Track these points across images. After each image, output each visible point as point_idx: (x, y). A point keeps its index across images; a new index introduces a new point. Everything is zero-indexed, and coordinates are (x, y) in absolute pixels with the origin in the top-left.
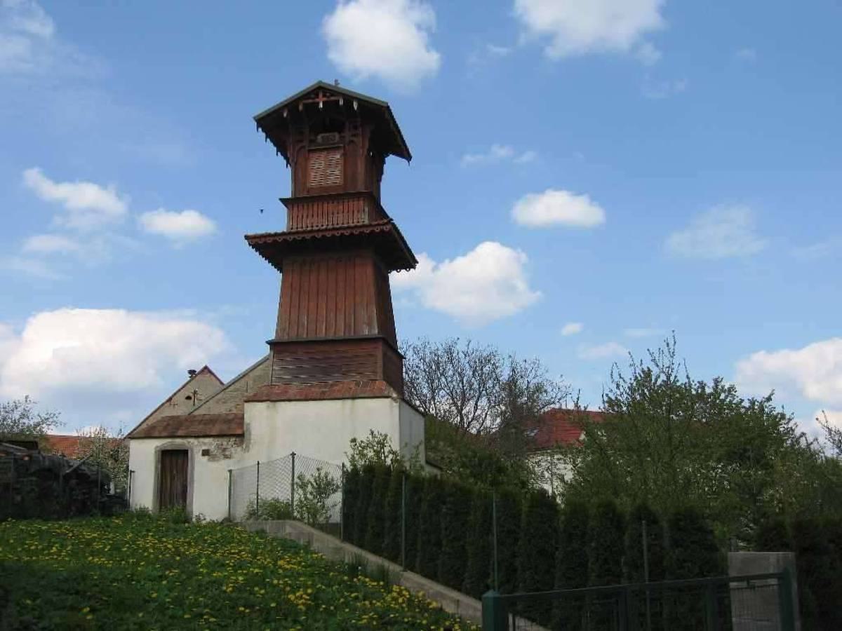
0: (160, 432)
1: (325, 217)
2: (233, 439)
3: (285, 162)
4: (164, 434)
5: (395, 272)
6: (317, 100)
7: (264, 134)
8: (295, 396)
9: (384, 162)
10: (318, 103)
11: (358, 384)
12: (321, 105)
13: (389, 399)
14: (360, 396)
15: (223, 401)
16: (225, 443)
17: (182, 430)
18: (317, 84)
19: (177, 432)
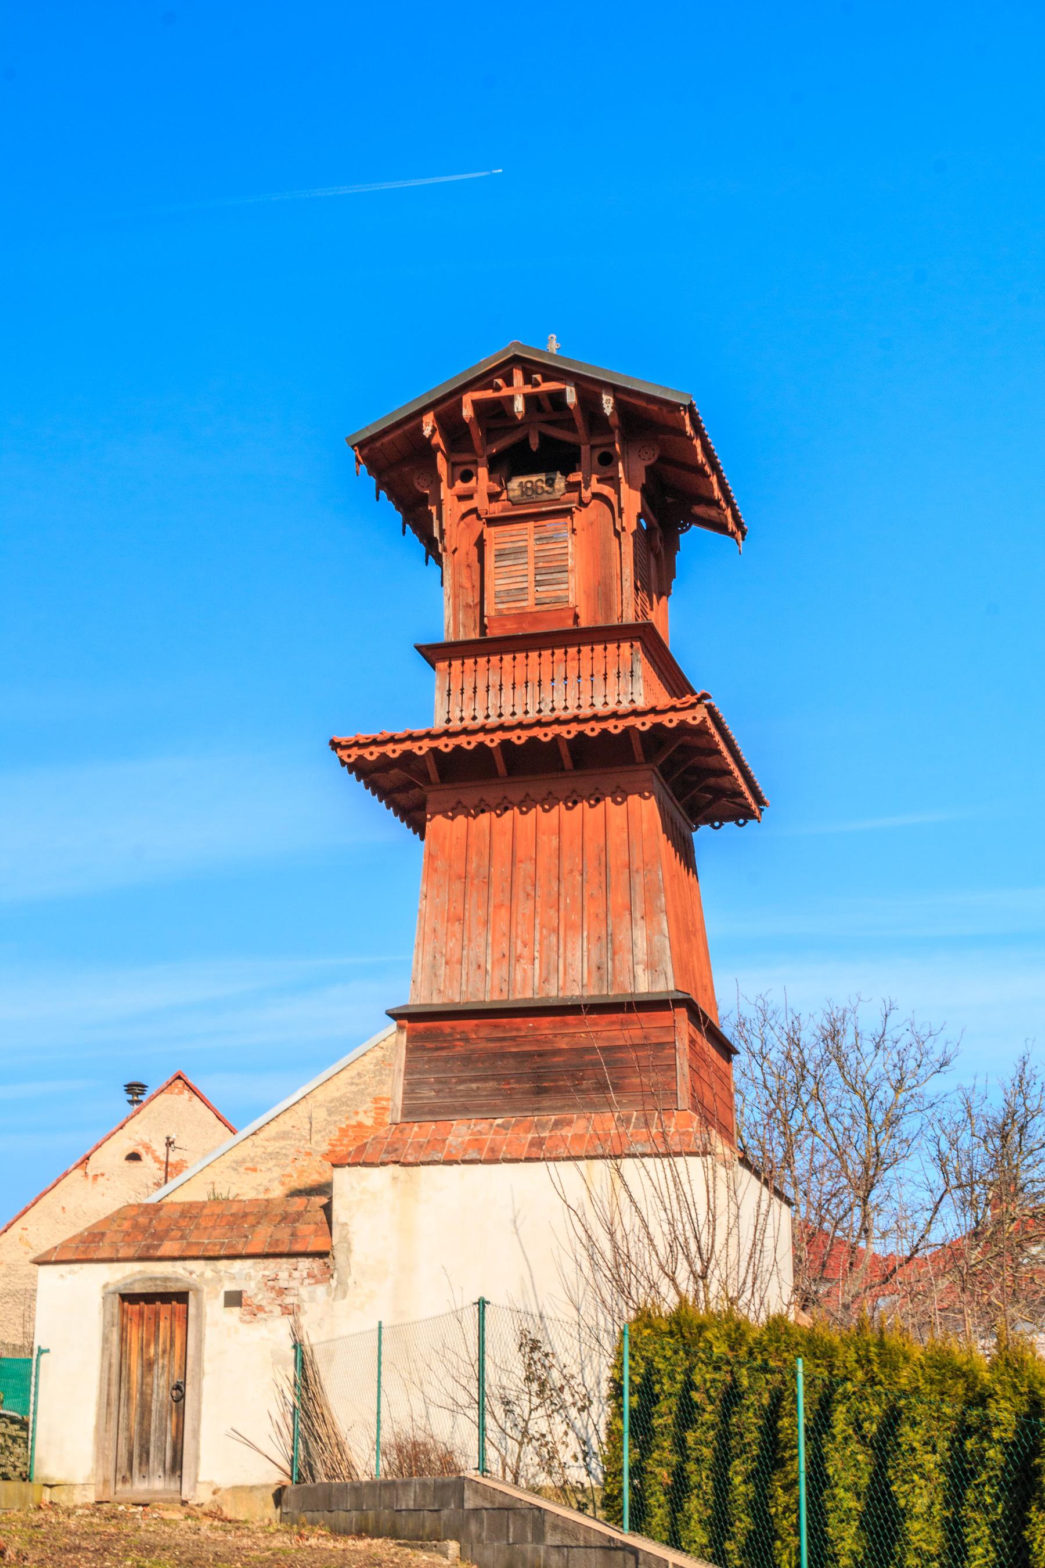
0: (113, 1245)
1: (585, 684)
2: (304, 1264)
3: (423, 548)
4: (131, 1252)
5: (732, 824)
6: (506, 392)
7: (373, 481)
8: (465, 1150)
10: (511, 399)
12: (519, 405)
15: (249, 1165)
16: (283, 1275)
17: (172, 1240)
18: (507, 351)
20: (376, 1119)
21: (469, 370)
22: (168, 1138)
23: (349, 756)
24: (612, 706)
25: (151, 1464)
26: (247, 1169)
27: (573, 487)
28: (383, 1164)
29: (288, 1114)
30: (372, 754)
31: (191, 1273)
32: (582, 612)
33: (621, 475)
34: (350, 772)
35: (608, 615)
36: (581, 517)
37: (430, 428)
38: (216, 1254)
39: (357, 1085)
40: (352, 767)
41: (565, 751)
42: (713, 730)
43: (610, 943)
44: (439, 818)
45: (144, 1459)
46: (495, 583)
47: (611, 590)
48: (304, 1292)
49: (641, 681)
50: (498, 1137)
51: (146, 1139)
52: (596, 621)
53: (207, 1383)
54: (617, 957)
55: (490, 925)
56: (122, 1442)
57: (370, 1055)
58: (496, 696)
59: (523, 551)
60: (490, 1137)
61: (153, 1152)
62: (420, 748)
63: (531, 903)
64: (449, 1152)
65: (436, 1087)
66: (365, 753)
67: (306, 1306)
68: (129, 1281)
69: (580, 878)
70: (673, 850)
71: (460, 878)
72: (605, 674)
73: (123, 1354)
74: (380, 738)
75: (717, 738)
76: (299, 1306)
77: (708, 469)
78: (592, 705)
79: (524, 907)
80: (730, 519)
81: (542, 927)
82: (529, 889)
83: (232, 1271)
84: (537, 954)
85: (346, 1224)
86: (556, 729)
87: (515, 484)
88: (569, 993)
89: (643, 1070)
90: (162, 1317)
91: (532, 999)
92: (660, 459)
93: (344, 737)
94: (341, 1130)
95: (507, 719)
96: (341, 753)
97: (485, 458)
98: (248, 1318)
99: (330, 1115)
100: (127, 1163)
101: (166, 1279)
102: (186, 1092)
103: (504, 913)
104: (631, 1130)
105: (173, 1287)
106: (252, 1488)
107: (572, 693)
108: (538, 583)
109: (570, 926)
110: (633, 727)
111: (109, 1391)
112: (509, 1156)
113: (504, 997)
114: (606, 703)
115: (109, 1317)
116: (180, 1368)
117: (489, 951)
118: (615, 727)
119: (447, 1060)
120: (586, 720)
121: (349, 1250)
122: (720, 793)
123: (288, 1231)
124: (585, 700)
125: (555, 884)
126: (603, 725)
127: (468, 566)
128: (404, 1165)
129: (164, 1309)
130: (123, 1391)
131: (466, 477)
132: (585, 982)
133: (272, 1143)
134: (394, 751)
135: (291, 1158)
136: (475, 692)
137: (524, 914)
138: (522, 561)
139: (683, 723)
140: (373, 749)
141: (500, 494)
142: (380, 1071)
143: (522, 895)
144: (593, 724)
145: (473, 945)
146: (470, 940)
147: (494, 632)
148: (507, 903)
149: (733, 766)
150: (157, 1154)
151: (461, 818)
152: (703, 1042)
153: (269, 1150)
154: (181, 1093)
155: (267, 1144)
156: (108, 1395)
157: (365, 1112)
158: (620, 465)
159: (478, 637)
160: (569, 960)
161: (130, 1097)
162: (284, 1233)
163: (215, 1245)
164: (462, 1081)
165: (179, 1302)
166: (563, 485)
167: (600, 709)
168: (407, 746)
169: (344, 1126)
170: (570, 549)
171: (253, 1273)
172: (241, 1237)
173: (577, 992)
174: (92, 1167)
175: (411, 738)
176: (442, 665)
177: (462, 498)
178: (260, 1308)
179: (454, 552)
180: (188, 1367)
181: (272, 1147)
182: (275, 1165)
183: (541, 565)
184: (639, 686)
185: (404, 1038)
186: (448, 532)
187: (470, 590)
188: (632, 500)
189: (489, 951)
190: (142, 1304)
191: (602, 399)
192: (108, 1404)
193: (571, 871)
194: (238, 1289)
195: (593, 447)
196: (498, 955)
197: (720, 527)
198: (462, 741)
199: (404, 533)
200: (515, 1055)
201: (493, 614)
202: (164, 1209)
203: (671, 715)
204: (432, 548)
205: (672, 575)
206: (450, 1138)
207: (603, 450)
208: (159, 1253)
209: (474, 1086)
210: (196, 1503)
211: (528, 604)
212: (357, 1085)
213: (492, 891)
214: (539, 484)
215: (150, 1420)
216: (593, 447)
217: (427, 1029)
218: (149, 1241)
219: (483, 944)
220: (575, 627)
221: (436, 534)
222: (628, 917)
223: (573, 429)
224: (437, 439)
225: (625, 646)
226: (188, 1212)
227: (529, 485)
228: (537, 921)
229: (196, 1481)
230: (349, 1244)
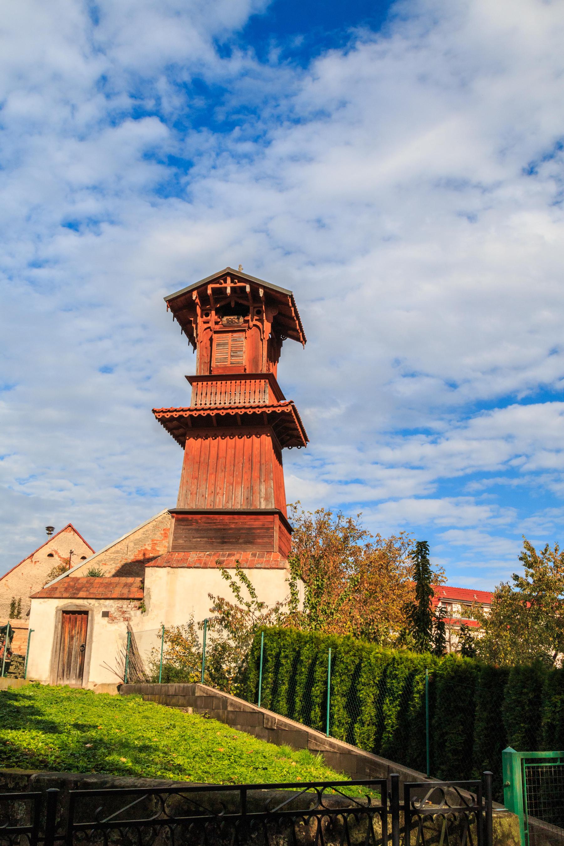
5: (296, 448)
6: (224, 285)
7: (172, 314)
8: (195, 563)
9: (281, 345)
10: (226, 288)
11: (254, 555)
12: (229, 291)
13: (285, 570)
14: (257, 566)
15: (104, 562)
17: (83, 591)
18: (225, 270)
19: (78, 594)
20: (152, 547)
21: (211, 276)
22: (71, 550)
23: (159, 416)
24: (257, 404)
25: (71, 674)
26: (103, 564)
27: (246, 322)
28: (165, 567)
29: (119, 544)
30: (168, 415)
31: (90, 604)
32: (247, 367)
33: (264, 318)
34: (159, 422)
35: (257, 369)
36: (249, 333)
37: (195, 296)
38: (100, 597)
39: (146, 534)
40: (159, 420)
41: (239, 419)
42: (293, 414)
43: (251, 489)
44: (192, 439)
45: (68, 673)
46: (216, 355)
47: (258, 360)
48: (132, 613)
49: (268, 394)
50: (207, 559)
51: (56, 549)
52: (252, 372)
53: (94, 645)
54: (254, 495)
55: (208, 481)
56: (60, 665)
57: (151, 524)
58: (214, 396)
59: (227, 344)
60: (204, 558)
61: (58, 554)
62: (186, 414)
63: (223, 473)
64: (189, 564)
65: (185, 539)
66: (165, 415)
67: (133, 618)
68: (66, 606)
69: (242, 465)
70: (275, 458)
71: (197, 463)
72: (255, 391)
73: (62, 633)
74: (171, 410)
75: (295, 417)
76: (130, 618)
77: (295, 318)
78: (249, 402)
79: (221, 475)
80: (301, 337)
81: (227, 482)
82: (223, 468)
83: (106, 604)
84: (225, 492)
85: (149, 588)
86: (237, 411)
87: (225, 319)
88: (236, 507)
89: (262, 537)
90: (78, 620)
91: (222, 509)
92: (279, 314)
93: (158, 408)
94: (139, 551)
95: (218, 405)
96: (156, 414)
97: (214, 309)
98: (111, 621)
99: (135, 545)
100: (48, 558)
101: (80, 606)
102: (72, 532)
103: (213, 476)
104: (256, 559)
105: (83, 609)
106: (109, 685)
107: (242, 397)
108: (232, 356)
109: (237, 483)
110: (265, 411)
111: (56, 646)
112: (211, 566)
113: (212, 507)
114: (254, 402)
115: (57, 619)
116: (84, 639)
117: (207, 490)
118: (258, 411)
119: (189, 530)
120: (248, 408)
121: (150, 598)
122: (292, 436)
123: (127, 590)
124: (247, 400)
125: (232, 467)
126: (254, 410)
127: (206, 348)
128: (172, 567)
129: (79, 617)
130: (62, 647)
131: (207, 315)
132: (242, 503)
133: (113, 555)
134: (176, 415)
135: (119, 561)
136: (206, 395)
137: (220, 477)
138: (226, 348)
139: (283, 411)
140: (168, 413)
141: (219, 322)
142: (155, 530)
143: (220, 471)
144: (250, 409)
145: (201, 487)
146: (200, 486)
147: (215, 373)
148: (215, 473)
149: (299, 427)
150: (60, 554)
151: (200, 440)
152: (283, 528)
153: (111, 557)
154: (70, 532)
155: (111, 555)
156: (56, 648)
157: (148, 545)
158: (264, 314)
159: (208, 374)
160: (236, 495)
161: (48, 532)
162: (125, 591)
163: (99, 594)
164: (194, 538)
165: (84, 614)
166: (242, 320)
167: (252, 404)
168: (181, 413)
169: (140, 549)
170: (244, 345)
171: (113, 605)
172: (109, 591)
173: (239, 507)
174: (34, 559)
175: (183, 410)
176: (195, 384)
177: (205, 323)
178: (115, 618)
179: (201, 342)
180: (87, 639)
181: (113, 556)
182: (113, 563)
183: (233, 349)
184: (267, 396)
185: (174, 520)
186: (199, 335)
187: (206, 357)
188: (267, 326)
189: (207, 490)
190: (71, 614)
191: (259, 291)
192: (56, 651)
193: (239, 463)
194: (107, 611)
195: (254, 308)
196: (210, 492)
197: (298, 339)
198: (202, 412)
199: (182, 333)
200: (215, 529)
201: (214, 366)
202: (80, 580)
203: (279, 408)
204: (192, 340)
205: (279, 355)
206: (190, 558)
207: (257, 309)
208: (78, 596)
209: (199, 539)
210: (87, 689)
211: (228, 364)
212: (146, 534)
213: (209, 468)
214: (234, 319)
215: (71, 658)
216: (254, 308)
217: (183, 518)
218: (74, 591)
219: (205, 488)
220: (244, 373)
221: (195, 335)
222: (259, 481)
223: (248, 300)
224: (198, 301)
225: (263, 381)
226: (89, 581)
227: (230, 320)
228: (225, 480)
229: (88, 681)
230: (150, 596)
